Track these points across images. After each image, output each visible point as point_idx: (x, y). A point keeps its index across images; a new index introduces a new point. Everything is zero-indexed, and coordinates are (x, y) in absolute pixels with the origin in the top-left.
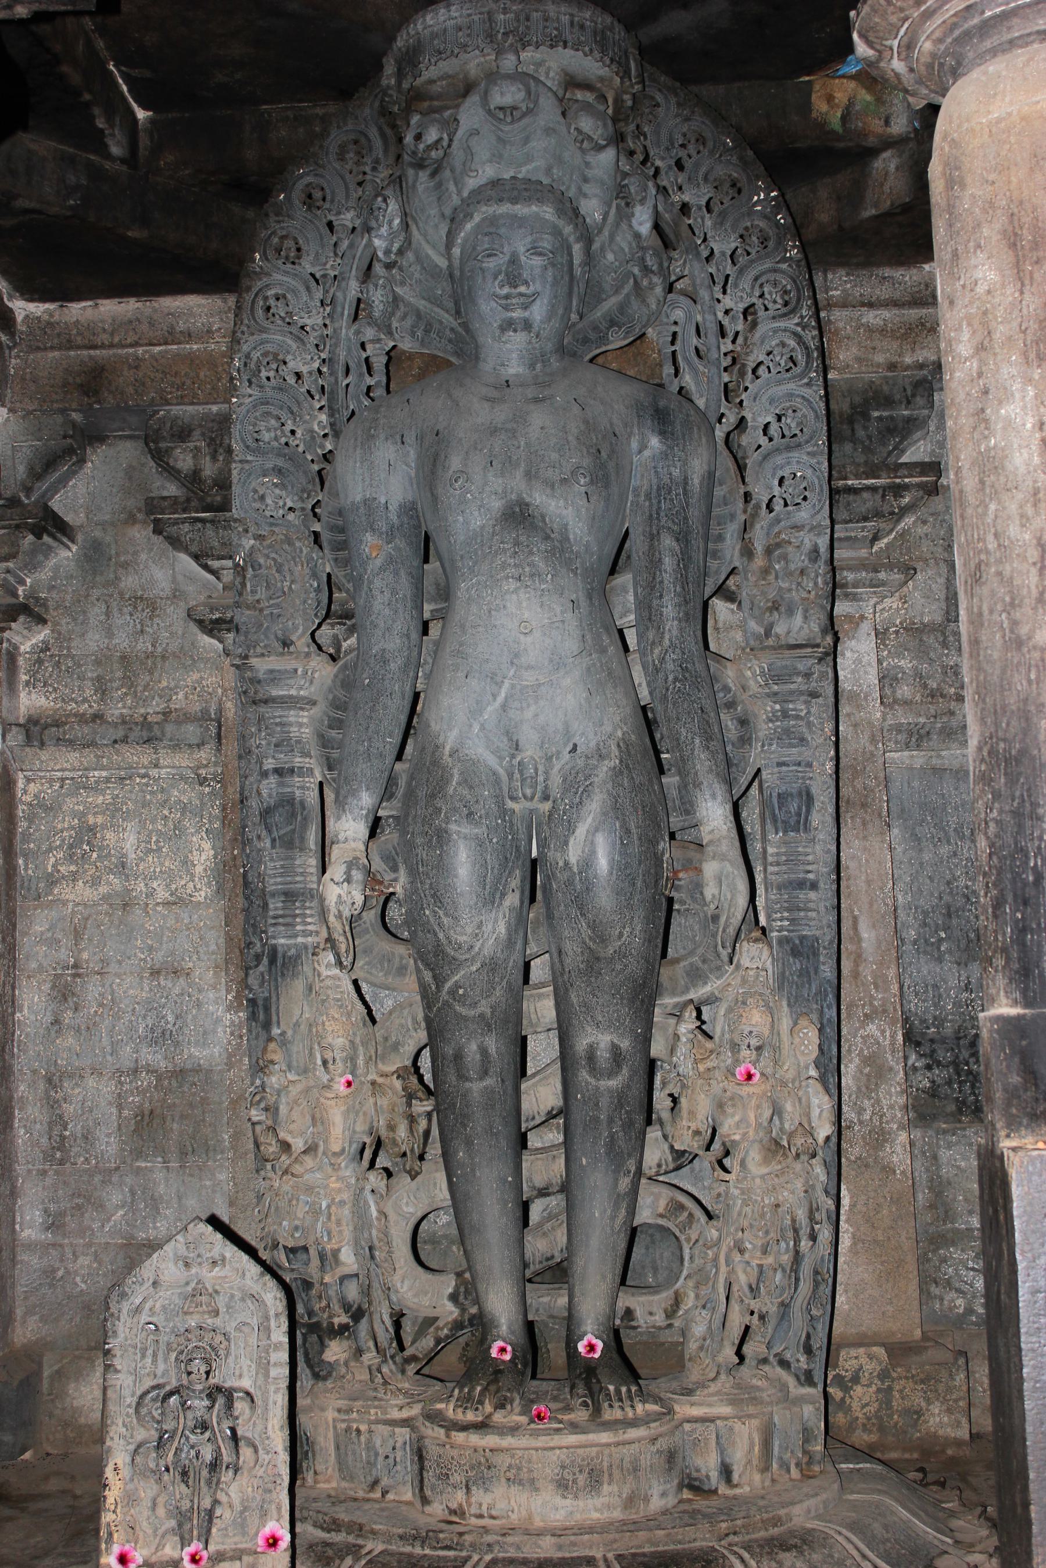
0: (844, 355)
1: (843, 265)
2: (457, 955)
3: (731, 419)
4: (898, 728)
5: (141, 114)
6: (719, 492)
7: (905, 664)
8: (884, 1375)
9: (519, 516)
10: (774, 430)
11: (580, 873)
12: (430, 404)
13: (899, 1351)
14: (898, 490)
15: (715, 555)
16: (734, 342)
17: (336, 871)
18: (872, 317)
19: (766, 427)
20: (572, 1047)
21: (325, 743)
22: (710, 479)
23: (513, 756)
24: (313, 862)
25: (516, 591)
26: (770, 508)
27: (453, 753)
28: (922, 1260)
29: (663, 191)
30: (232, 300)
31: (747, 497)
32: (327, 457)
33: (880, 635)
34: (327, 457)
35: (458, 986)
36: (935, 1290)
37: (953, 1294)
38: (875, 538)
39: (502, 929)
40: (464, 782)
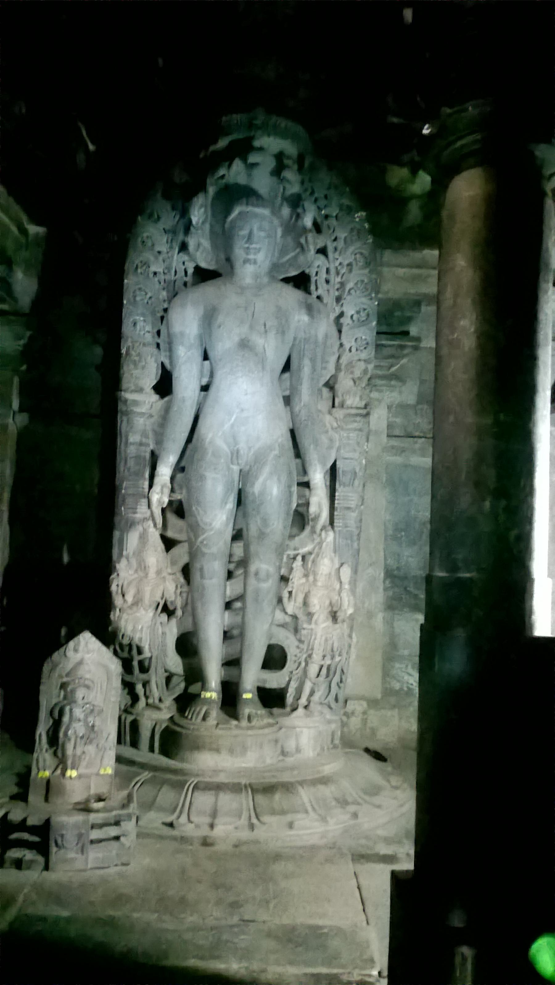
0: (385, 287)
1: (390, 248)
2: (273, 832)
3: (338, 311)
4: (393, 447)
5: (91, 147)
6: (329, 343)
7: (398, 420)
8: (364, 713)
9: (244, 345)
10: (355, 317)
11: (259, 497)
12: (209, 289)
13: (373, 703)
14: (402, 347)
15: (325, 368)
16: (342, 277)
17: (157, 488)
18: (401, 272)
19: (352, 317)
20: (171, 332)
21: (155, 433)
22: (326, 336)
23: (235, 446)
24: (147, 483)
25: (242, 377)
26: (350, 350)
27: (210, 443)
28: (384, 667)
29: (320, 209)
30: (431, 254)
31: (341, 345)
32: (166, 310)
33: (389, 408)
34: (166, 310)
35: (204, 540)
36: (388, 679)
37: (395, 681)
38: (392, 366)
39: (224, 517)
40: (214, 454)
